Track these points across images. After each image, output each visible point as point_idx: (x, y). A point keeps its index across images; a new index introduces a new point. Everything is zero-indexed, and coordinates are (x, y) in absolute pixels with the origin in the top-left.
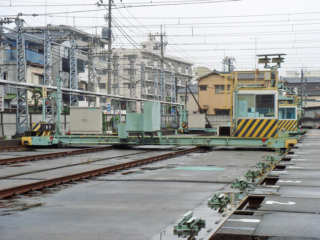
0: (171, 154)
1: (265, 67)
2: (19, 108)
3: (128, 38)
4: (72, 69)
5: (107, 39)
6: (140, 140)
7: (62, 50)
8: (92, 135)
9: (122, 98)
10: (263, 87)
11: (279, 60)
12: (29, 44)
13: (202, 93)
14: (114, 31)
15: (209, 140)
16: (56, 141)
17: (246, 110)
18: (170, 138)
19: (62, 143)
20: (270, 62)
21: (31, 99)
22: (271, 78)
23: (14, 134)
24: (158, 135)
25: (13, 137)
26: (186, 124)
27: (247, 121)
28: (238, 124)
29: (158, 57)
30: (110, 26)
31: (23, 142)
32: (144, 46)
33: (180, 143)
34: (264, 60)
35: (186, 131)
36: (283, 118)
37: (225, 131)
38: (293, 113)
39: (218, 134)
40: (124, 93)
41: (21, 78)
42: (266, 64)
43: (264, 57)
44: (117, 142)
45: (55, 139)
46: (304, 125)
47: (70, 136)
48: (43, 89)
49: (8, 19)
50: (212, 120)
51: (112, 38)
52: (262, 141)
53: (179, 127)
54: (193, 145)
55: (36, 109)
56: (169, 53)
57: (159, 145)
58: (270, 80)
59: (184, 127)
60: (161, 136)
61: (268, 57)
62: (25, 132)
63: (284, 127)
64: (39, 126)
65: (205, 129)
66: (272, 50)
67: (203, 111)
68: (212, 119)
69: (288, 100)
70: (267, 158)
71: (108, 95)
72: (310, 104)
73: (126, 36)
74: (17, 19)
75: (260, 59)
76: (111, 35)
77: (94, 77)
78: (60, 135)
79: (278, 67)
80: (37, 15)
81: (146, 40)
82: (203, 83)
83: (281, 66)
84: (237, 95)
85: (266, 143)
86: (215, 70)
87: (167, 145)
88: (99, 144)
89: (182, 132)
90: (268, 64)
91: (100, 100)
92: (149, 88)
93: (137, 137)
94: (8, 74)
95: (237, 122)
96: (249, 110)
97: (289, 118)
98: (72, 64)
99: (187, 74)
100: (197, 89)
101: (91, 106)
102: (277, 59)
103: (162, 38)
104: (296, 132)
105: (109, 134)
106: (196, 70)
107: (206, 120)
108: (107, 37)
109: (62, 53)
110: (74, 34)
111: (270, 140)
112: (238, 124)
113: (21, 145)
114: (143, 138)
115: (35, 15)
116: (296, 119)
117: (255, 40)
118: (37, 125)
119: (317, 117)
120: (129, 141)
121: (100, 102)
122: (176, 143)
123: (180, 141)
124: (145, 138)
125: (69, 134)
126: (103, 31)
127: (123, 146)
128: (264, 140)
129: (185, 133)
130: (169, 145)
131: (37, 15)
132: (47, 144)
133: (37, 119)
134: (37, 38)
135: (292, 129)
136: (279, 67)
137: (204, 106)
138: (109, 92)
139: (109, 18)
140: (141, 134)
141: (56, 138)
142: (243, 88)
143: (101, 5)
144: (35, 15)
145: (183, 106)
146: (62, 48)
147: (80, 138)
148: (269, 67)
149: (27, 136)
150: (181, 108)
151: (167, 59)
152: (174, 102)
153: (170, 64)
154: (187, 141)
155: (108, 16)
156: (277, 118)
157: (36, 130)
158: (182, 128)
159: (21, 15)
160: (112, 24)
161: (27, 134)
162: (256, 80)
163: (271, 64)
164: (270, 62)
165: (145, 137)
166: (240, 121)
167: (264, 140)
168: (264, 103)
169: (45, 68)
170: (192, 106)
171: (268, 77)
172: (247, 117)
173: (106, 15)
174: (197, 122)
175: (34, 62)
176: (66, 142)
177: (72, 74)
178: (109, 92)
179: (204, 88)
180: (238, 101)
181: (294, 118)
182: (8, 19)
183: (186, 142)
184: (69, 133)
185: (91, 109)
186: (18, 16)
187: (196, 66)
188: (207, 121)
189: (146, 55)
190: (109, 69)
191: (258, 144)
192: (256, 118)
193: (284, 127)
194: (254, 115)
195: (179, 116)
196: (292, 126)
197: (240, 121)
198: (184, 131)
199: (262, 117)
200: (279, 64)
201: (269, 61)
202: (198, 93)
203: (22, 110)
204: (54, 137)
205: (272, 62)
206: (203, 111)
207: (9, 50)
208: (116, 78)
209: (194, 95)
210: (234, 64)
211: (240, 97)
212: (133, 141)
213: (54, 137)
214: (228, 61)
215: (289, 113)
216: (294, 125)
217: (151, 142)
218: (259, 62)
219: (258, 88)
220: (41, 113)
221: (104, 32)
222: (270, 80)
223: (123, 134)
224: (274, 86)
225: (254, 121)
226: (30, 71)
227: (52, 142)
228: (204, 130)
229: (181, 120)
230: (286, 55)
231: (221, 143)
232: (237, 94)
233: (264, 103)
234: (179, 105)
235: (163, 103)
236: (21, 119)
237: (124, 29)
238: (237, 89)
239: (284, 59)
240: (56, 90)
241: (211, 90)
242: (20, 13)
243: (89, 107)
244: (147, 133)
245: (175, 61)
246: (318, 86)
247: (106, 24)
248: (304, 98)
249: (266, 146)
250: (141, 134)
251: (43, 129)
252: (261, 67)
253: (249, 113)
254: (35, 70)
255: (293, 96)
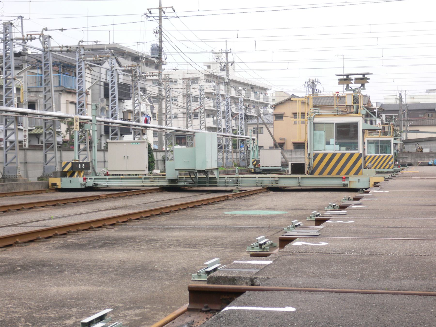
0: (227, 196)
1: (347, 89)
2: (46, 144)
3: (183, 55)
4: (112, 94)
5: (157, 58)
6: (193, 181)
7: (103, 72)
8: (136, 175)
9: (177, 131)
10: (344, 114)
11: (363, 80)
12: (63, 66)
13: (278, 123)
14: (166, 47)
15: (277, 179)
16: (90, 183)
17: (324, 142)
18: (229, 178)
19: (97, 185)
20: (352, 83)
21: (65, 133)
22: (354, 103)
23: (40, 175)
24: (214, 175)
25: (39, 178)
26: (257, 162)
27: (325, 155)
28: (314, 160)
29: (222, 79)
30: (161, 41)
31: (50, 184)
32: (209, 67)
33: (241, 183)
34: (346, 80)
35: (258, 170)
36: (377, 152)
37: (298, 169)
38: (388, 146)
39: (290, 173)
40: (178, 125)
41: (48, 106)
42: (348, 85)
43: (345, 77)
44: (164, 184)
45: (89, 180)
46: (403, 161)
47: (107, 177)
48: (75, 119)
49: (31, 36)
50: (290, 157)
51: (163, 57)
52: (341, 179)
53: (249, 165)
54: (257, 186)
55: (67, 146)
56: (237, 74)
57: (216, 186)
58: (352, 104)
59: (255, 165)
60: (218, 176)
61: (349, 77)
62: (54, 172)
63: (370, 162)
64: (70, 165)
65: (281, 168)
66: (354, 69)
67: (278, 146)
68: (291, 155)
69: (369, 130)
70: (344, 200)
71: (159, 126)
72: (412, 136)
73: (180, 53)
74: (42, 35)
75: (340, 80)
76: (161, 53)
77: (139, 104)
78: (96, 175)
79: (362, 89)
80: (65, 30)
81: (211, 58)
82: (279, 111)
83: (366, 87)
84: (312, 124)
85: (346, 182)
86: (293, 95)
87: (226, 186)
88: (143, 186)
89: (253, 171)
90: (350, 85)
91: (154, 134)
92: (215, 118)
93: (189, 176)
94: (37, 102)
95: (312, 157)
96: (328, 143)
97: (385, 153)
98: (111, 89)
99: (262, 100)
100: (271, 119)
101: (136, 140)
102: (361, 79)
103: (227, 56)
104: (393, 170)
105: (156, 174)
106: (274, 95)
107: (282, 157)
108: (157, 56)
109: (103, 76)
110: (119, 52)
111: (351, 179)
112: (314, 160)
113: (48, 188)
114: (196, 177)
115: (62, 30)
116: (393, 154)
117: (342, 57)
118: (68, 163)
119: (418, 151)
120: (180, 182)
121: (154, 136)
122: (237, 183)
123: (241, 181)
124: (199, 178)
125: (107, 174)
126: (152, 49)
127: (173, 187)
128: (344, 179)
129: (255, 173)
130: (227, 186)
131: (65, 30)
132: (79, 187)
133: (70, 157)
134: (67, 58)
135: (388, 166)
136: (364, 89)
137: (281, 139)
138: (160, 123)
139: (160, 32)
140: (194, 173)
141: (90, 179)
142: (319, 115)
143: (149, 17)
144: (62, 30)
145: (254, 139)
146: (103, 71)
147: (119, 178)
148: (352, 89)
149: (56, 177)
150: (252, 142)
151: (233, 81)
152: (243, 135)
153: (240, 88)
154: (250, 181)
155: (158, 29)
156: (361, 151)
157: (66, 169)
158: (253, 167)
159: (46, 30)
160: (163, 39)
161: (55, 175)
162: (335, 106)
163: (354, 85)
164: (352, 83)
165: (198, 176)
166: (316, 156)
167: (344, 179)
168: (346, 133)
169: (77, 94)
170: (265, 140)
171: (349, 101)
172: (325, 150)
173: (155, 29)
174: (271, 158)
175: (70, 88)
176: (102, 184)
177: (112, 101)
178: (160, 123)
179: (279, 117)
180: (314, 130)
181: (390, 153)
182: (31, 36)
183: (248, 183)
184: (107, 172)
185: (136, 144)
186: (43, 31)
187: (273, 90)
188: (284, 157)
189: (210, 77)
190: (160, 94)
191: (338, 183)
192: (336, 152)
193: (370, 162)
194: (334, 149)
195: (248, 151)
196: (388, 163)
197: (316, 156)
198: (255, 170)
199: (343, 150)
200: (363, 85)
201: (351, 81)
202: (272, 124)
203: (49, 146)
204: (88, 178)
205: (355, 83)
206: (280, 145)
207: (39, 74)
208: (168, 105)
209: (268, 126)
210: (319, 87)
211: (315, 126)
212: (184, 182)
213: (88, 178)
214: (312, 84)
215: (383, 147)
216: (390, 161)
217: (206, 183)
218: (339, 84)
219: (338, 114)
220: (73, 150)
221: (153, 50)
222: (352, 104)
223: (171, 174)
224: (357, 112)
225: (334, 155)
226: (64, 98)
227: (85, 184)
228: (280, 169)
229: (251, 156)
230: (372, 74)
231: (292, 183)
232: (312, 122)
233: (346, 133)
234: (249, 138)
235: (228, 136)
236: (49, 157)
237: (178, 44)
238: (312, 117)
239: (368, 79)
240: (91, 121)
241: (288, 120)
242: (45, 28)
243: (134, 141)
244: (200, 172)
245: (247, 85)
246: (422, 114)
247: (155, 39)
248: (404, 129)
249: (347, 185)
250: (194, 173)
251: (74, 169)
252: (341, 89)
253: (327, 146)
254: (70, 98)
255: (388, 125)
